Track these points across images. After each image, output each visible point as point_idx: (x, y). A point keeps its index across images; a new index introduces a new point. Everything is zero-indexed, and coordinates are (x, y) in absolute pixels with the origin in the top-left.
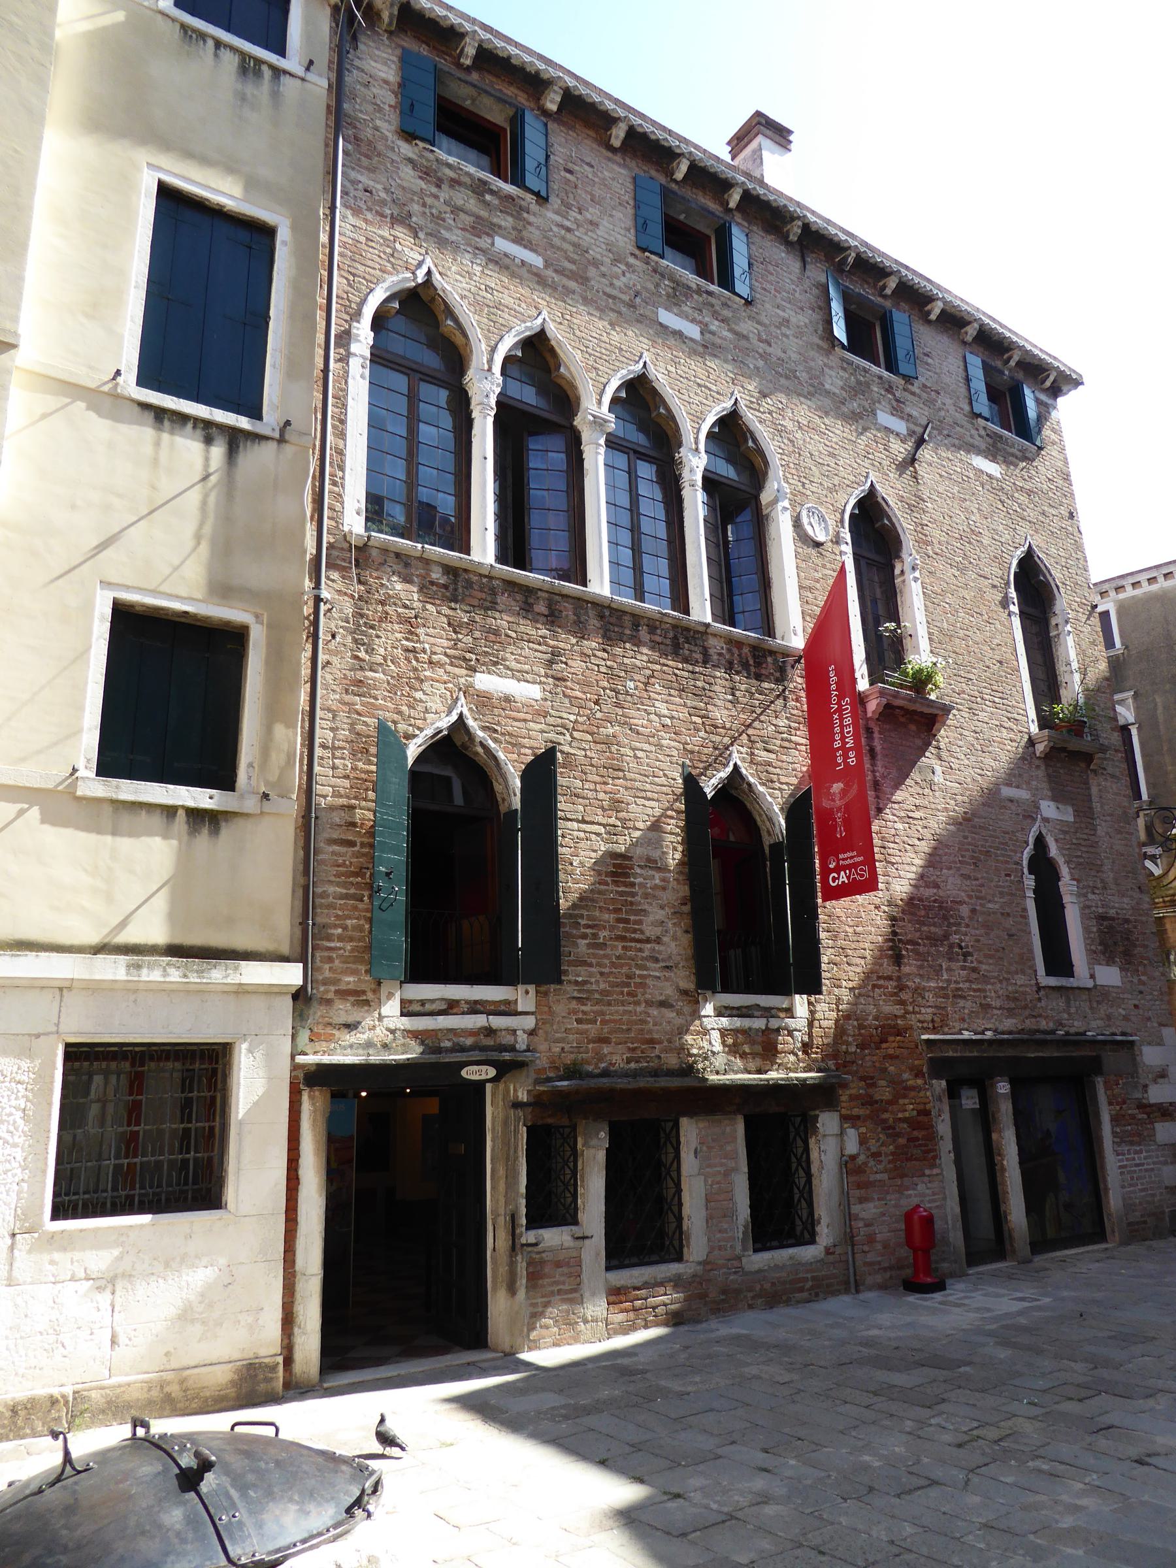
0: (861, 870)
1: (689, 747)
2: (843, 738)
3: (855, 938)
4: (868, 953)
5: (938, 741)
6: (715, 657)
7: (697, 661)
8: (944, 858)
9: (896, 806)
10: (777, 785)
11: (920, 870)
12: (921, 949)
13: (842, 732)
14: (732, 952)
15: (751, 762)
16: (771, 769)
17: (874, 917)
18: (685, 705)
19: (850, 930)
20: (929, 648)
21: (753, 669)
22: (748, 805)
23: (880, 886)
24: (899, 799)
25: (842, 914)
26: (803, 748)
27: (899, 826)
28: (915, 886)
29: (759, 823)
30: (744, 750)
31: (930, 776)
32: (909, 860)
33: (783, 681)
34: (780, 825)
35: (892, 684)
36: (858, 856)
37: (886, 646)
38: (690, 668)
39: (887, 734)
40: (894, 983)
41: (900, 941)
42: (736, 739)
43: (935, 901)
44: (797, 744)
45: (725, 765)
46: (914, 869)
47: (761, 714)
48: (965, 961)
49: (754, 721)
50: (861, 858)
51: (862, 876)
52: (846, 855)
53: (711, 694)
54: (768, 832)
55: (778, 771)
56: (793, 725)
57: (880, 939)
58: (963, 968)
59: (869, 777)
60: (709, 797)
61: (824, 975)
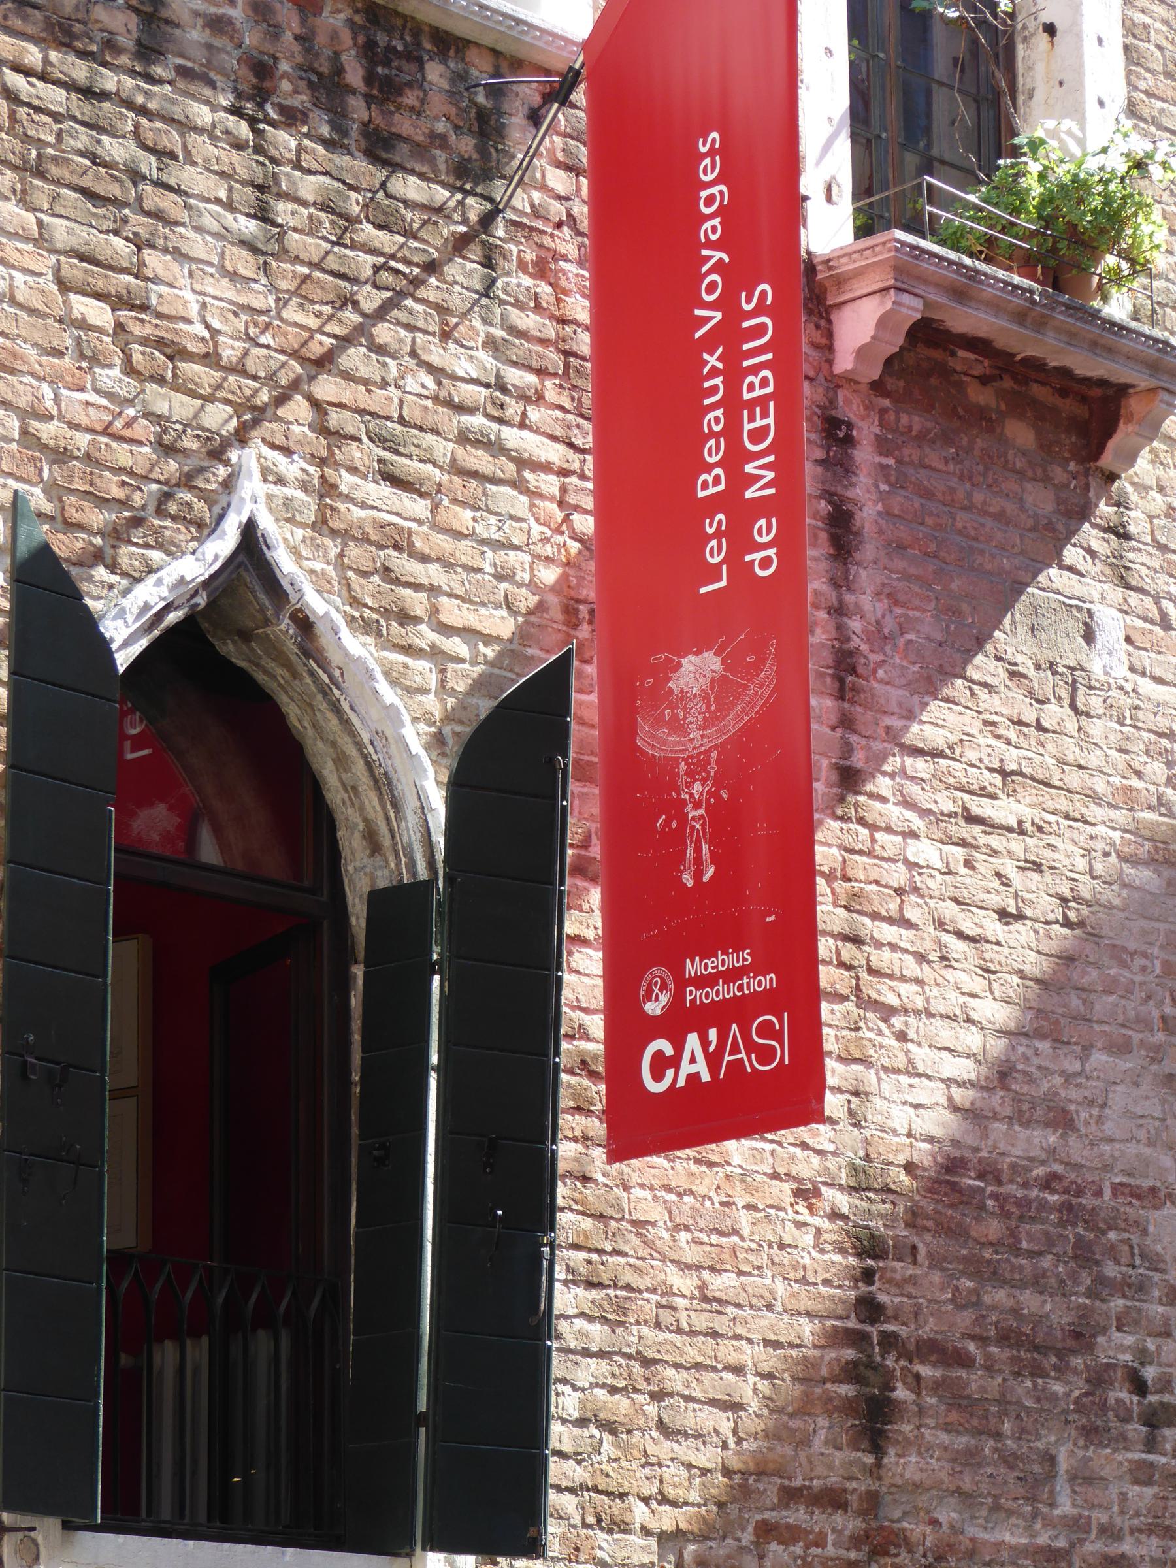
0: (766, 1030)
1: (48, 431)
2: (735, 458)
3: (702, 1321)
4: (748, 1389)
5: (1121, 503)
6: (196, 35)
7: (110, 45)
8: (1104, 1004)
9: (919, 766)
10: (425, 635)
11: (997, 1047)
12: (975, 1382)
13: (732, 431)
14: (166, 1355)
15: (321, 524)
16: (404, 565)
17: (790, 1234)
18: (42, 240)
19: (685, 1283)
20: (1118, 94)
21: (358, 109)
22: (293, 712)
23: (833, 1103)
24: (935, 737)
25: (656, 1213)
26: (550, 484)
27: (925, 851)
28: (970, 1114)
29: (335, 794)
30: (291, 468)
31: (1073, 651)
32: (953, 1001)
33: (487, 175)
34: (423, 809)
35: (954, 240)
36: (757, 969)
37: (941, 67)
38: (80, 71)
39: (910, 452)
40: (849, 1523)
41: (889, 1341)
42: (259, 415)
43: (1049, 1182)
44: (523, 463)
45: (205, 529)
46: (972, 1040)
47: (381, 314)
48: (1151, 1444)
49: (346, 341)
50: (768, 981)
51: (765, 1055)
52: (712, 965)
53: (166, 202)
54: (371, 837)
55: (433, 574)
56: (516, 377)
57: (807, 1329)
58: (1143, 1474)
59: (820, 636)
60: (123, 660)
61: (558, 1471)
